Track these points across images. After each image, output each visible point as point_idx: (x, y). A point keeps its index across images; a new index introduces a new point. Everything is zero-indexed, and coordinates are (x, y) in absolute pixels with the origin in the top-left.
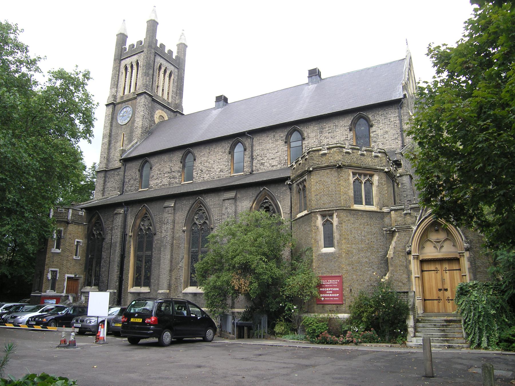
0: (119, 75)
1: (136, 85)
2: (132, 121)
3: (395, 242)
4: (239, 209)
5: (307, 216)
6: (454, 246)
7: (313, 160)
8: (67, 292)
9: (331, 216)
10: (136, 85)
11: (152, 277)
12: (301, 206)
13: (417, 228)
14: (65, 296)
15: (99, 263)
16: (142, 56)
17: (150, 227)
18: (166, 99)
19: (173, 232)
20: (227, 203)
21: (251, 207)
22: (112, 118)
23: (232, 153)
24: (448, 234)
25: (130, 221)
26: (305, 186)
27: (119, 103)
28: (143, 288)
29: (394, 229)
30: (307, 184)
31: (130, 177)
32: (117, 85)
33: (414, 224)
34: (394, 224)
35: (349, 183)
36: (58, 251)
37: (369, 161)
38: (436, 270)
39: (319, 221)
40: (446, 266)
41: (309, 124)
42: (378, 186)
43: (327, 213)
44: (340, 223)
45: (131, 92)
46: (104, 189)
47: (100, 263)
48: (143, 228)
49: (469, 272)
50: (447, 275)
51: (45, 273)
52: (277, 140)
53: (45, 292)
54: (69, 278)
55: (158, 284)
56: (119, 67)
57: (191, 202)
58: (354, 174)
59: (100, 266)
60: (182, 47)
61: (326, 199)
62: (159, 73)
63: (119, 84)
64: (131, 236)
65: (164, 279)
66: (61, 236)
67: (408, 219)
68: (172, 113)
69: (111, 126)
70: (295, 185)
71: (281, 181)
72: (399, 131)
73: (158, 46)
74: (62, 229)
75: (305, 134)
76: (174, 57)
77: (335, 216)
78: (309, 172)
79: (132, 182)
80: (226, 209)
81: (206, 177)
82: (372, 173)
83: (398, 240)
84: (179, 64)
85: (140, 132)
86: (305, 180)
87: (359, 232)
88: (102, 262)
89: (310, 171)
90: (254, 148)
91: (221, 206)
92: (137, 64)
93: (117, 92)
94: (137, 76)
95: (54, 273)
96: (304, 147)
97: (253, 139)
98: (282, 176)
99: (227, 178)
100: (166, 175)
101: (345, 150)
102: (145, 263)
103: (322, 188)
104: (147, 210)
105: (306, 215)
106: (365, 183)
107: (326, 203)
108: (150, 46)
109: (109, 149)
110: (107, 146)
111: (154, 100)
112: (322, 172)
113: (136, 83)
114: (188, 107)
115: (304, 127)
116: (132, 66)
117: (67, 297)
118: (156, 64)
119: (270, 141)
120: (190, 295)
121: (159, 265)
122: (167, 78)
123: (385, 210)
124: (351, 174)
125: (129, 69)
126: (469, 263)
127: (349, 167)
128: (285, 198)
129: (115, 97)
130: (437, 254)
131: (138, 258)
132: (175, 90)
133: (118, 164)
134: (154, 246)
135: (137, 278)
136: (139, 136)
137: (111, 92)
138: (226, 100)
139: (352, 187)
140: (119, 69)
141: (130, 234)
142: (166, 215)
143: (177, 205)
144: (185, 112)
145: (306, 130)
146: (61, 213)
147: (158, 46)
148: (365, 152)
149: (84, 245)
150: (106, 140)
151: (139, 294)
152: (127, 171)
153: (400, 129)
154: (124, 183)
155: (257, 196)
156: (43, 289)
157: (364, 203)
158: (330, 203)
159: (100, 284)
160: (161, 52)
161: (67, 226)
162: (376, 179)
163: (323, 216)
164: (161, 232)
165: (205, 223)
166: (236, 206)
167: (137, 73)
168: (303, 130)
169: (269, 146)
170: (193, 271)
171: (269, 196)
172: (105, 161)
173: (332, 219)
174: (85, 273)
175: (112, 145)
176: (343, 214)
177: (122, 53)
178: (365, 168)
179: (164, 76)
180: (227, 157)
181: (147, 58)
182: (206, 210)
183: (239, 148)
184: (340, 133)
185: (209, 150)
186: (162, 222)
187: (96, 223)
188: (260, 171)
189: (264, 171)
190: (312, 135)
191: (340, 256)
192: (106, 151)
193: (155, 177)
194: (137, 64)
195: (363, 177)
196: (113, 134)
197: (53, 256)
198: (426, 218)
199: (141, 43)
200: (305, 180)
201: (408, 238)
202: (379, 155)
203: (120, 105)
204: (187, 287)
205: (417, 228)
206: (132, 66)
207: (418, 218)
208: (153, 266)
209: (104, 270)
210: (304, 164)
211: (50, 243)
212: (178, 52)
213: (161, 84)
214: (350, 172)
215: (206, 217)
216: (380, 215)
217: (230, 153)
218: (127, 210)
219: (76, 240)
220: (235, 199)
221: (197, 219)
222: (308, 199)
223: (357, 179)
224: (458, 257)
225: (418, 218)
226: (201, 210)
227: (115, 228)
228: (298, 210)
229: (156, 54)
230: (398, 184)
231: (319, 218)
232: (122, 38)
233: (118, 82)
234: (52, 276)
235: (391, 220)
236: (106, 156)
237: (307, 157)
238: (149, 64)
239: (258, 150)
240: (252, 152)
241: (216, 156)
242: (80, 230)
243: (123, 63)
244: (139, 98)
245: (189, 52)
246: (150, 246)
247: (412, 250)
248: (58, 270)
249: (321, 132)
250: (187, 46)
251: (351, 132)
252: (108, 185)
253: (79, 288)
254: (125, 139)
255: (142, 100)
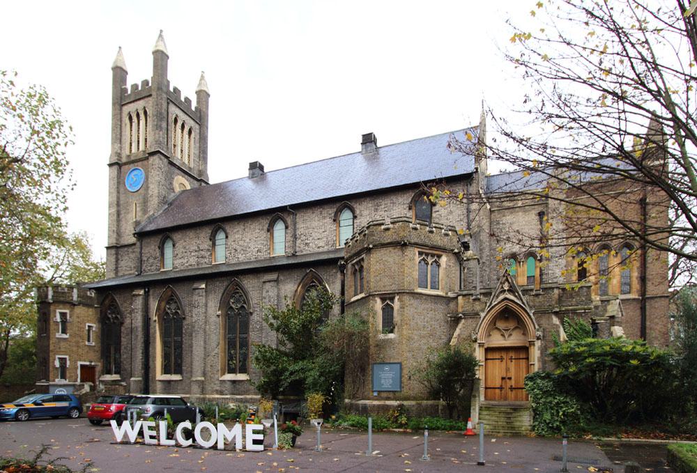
0: (121, 126)
1: (146, 141)
2: (146, 186)
3: (460, 329)
4: (283, 294)
5: (364, 300)
6: (524, 334)
7: (374, 236)
8: (82, 380)
9: (392, 299)
10: (146, 141)
11: (184, 364)
12: (356, 288)
13: (486, 315)
14: (80, 385)
15: (118, 350)
16: (150, 102)
17: (178, 311)
18: (186, 162)
19: (206, 317)
20: (268, 286)
21: (296, 291)
22: (119, 183)
23: (271, 231)
24: (518, 322)
25: (154, 305)
26: (362, 267)
27: (125, 164)
28: (238, 375)
29: (460, 315)
30: (365, 265)
31: (148, 255)
32: (121, 141)
33: (483, 310)
34: (460, 310)
35: (415, 264)
36: (64, 336)
37: (437, 239)
38: (502, 359)
39: (378, 305)
40: (512, 354)
41: (363, 200)
42: (446, 268)
43: (388, 296)
44: (402, 307)
45: (141, 149)
46: (117, 268)
47: (120, 350)
48: (169, 311)
49: (539, 361)
50: (512, 365)
51: (51, 361)
52: (324, 218)
53: (54, 381)
54: (82, 366)
55: (191, 372)
56: (121, 114)
57: (226, 284)
58: (420, 254)
59: (120, 352)
60: (203, 96)
61: (386, 281)
62: (175, 127)
63: (123, 138)
64: (155, 321)
65: (197, 365)
66: (66, 319)
67: (478, 307)
68: (196, 182)
69: (118, 192)
70: (349, 266)
71: (331, 263)
72: (465, 211)
73: (171, 90)
74: (67, 311)
75: (358, 212)
76: (193, 109)
77: (397, 298)
78: (368, 250)
79: (151, 260)
80: (267, 292)
81: (242, 258)
82: (441, 253)
83: (464, 328)
84: (200, 118)
85: (156, 202)
86: (363, 259)
87: (422, 317)
88: (123, 348)
89: (370, 249)
90: (297, 226)
91: (261, 289)
92: (145, 113)
93: (121, 148)
94: (146, 129)
95: (63, 361)
96: (355, 226)
97: (296, 215)
98: (332, 256)
99: (265, 260)
100: (193, 254)
101: (411, 225)
102: (175, 349)
103: (383, 268)
104: (173, 292)
105: (363, 298)
106: (431, 264)
107: (387, 286)
108: (159, 89)
109: (118, 220)
110: (115, 217)
111: (171, 163)
112: (383, 251)
113: (146, 139)
114: (214, 177)
115: (356, 203)
116: (138, 115)
117: (82, 386)
118: (170, 115)
119: (316, 218)
120: (228, 383)
121: (192, 351)
122: (186, 136)
123: (450, 295)
124: (417, 253)
125: (135, 119)
126: (539, 352)
127: (416, 245)
128: (334, 282)
129: (119, 155)
130: (504, 342)
131: (165, 344)
132: (197, 152)
133: (133, 240)
134: (184, 331)
135: (165, 365)
136: (156, 206)
137: (113, 148)
138: (261, 168)
139: (417, 268)
140: (121, 118)
141: (154, 319)
142: (196, 298)
143: (209, 287)
144: (211, 182)
145: (358, 207)
146: (63, 293)
147: (171, 90)
148: (434, 229)
149: (97, 330)
150: (114, 210)
151: (169, 382)
152: (144, 248)
153: (467, 209)
154: (141, 261)
155: (303, 279)
156: (51, 379)
157: (429, 286)
158: (391, 285)
159: (122, 372)
160: (176, 99)
161: (74, 308)
162: (444, 260)
163: (383, 300)
164: (192, 316)
165: (243, 307)
166: (279, 289)
167: (146, 123)
168: (355, 206)
169: (315, 224)
170: (231, 358)
171: (316, 279)
172: (115, 235)
173: (393, 303)
174: (102, 360)
175: (121, 216)
176: (406, 298)
177: (121, 98)
178: (433, 248)
179: (182, 132)
180: (264, 234)
181: (157, 105)
182: (245, 294)
183: (279, 228)
184: (399, 208)
185: (244, 226)
186: (192, 305)
187: (110, 305)
188: (304, 253)
189: (309, 252)
190: (366, 213)
191: (400, 343)
192: (115, 223)
193: (179, 256)
194: (145, 113)
195: (429, 257)
196: (122, 202)
197: (59, 342)
198: (496, 305)
199: (148, 84)
200: (363, 259)
201: (474, 325)
202: (450, 233)
203: (127, 166)
204: (224, 374)
205: (486, 315)
206: (138, 115)
207: (488, 304)
208: (184, 353)
209: (125, 356)
210: (362, 241)
211: (52, 327)
212: (198, 102)
213: (179, 143)
214: (417, 251)
215: (244, 301)
216: (448, 300)
217: (268, 231)
218: (149, 291)
219: (87, 324)
220: (277, 281)
221: (233, 303)
222: (365, 281)
223: (424, 259)
224: (527, 345)
225: (488, 304)
226: (238, 293)
227: (134, 311)
228: (353, 293)
229: (169, 101)
230: (464, 268)
231: (378, 300)
232: (119, 74)
233: (121, 136)
234: (61, 363)
235: (457, 307)
236: (115, 229)
237: (366, 232)
238: (156, 113)
239: (302, 227)
240: (295, 230)
241: (252, 234)
242: (91, 313)
243: (126, 109)
244: (151, 159)
245: (212, 102)
246: (179, 331)
247: (478, 337)
248: (67, 357)
249: (376, 210)
250: (209, 95)
251: (411, 211)
252: (122, 263)
253: (97, 377)
254: (138, 209)
255: (155, 160)
